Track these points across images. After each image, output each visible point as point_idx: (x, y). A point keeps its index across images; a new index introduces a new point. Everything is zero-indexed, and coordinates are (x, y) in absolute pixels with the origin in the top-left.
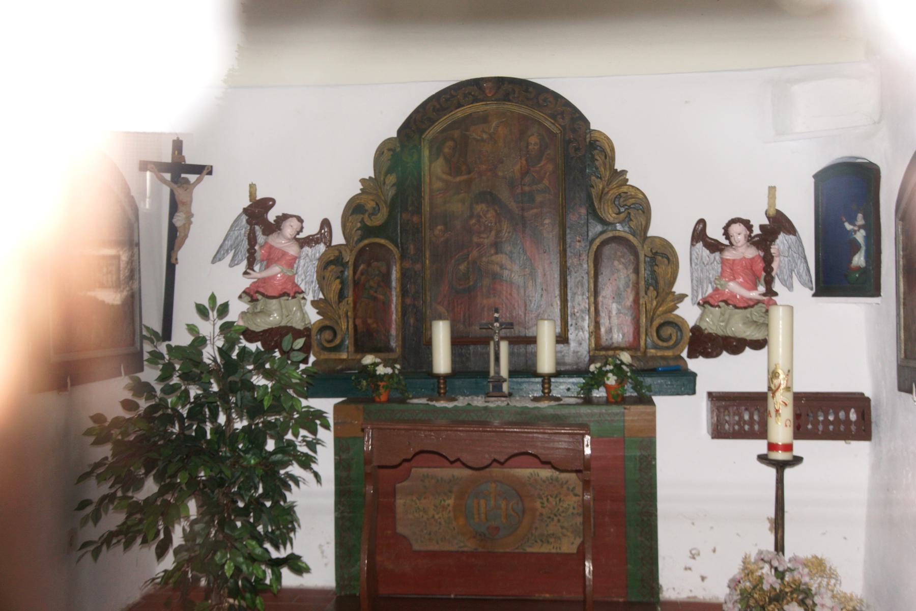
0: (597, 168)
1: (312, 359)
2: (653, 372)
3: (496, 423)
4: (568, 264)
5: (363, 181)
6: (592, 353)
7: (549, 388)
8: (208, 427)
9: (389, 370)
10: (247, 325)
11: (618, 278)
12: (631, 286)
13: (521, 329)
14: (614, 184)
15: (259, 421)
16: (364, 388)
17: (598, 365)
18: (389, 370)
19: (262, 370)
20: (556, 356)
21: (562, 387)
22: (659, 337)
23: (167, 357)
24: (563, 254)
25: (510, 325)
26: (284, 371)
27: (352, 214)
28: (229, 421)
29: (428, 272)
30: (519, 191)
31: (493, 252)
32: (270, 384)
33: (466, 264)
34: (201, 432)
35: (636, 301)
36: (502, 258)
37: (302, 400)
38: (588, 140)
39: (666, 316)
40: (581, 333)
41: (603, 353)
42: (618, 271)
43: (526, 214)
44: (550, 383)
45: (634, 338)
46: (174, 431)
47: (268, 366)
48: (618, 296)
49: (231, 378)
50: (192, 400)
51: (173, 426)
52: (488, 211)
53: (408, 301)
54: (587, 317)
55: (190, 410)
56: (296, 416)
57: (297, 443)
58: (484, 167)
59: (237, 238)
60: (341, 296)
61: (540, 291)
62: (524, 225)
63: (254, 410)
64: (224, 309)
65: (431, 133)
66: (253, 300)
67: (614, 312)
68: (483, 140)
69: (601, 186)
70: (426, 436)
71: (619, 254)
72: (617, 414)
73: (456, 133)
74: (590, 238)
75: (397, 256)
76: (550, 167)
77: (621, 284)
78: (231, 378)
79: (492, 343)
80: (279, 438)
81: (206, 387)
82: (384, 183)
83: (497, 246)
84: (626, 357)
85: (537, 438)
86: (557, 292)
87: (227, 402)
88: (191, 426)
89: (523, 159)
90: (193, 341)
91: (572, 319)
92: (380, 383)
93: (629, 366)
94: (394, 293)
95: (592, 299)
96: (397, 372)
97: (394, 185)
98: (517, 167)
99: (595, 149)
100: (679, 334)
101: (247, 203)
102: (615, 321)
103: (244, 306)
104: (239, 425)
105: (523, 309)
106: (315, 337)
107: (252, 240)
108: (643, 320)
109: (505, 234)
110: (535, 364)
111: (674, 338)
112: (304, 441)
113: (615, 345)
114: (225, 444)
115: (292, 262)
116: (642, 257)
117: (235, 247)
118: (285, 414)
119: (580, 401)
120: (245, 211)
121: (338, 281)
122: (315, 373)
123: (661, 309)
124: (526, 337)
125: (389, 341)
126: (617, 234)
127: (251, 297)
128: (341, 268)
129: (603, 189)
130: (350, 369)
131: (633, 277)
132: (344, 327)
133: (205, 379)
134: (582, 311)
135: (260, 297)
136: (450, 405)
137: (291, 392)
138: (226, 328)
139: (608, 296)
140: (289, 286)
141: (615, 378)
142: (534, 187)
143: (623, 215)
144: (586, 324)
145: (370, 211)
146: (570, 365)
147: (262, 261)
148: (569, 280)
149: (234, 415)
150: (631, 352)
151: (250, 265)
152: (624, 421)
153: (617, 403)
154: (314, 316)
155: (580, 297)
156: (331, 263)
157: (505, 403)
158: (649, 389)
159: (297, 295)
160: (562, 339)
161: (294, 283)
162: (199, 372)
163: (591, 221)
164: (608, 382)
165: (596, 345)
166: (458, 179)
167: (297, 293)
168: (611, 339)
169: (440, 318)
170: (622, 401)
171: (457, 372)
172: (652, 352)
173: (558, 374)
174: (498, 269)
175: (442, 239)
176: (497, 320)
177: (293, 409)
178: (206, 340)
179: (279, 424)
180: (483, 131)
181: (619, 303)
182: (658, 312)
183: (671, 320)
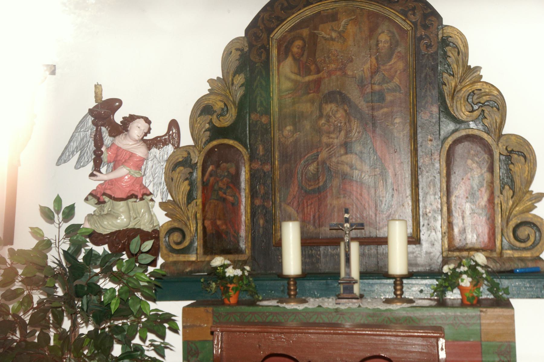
0: (449, 65)
1: (160, 261)
2: (510, 273)
3: (348, 325)
4: (420, 164)
5: (211, 81)
6: (445, 254)
7: (401, 290)
8: (52, 333)
9: (239, 272)
10: (93, 228)
11: (471, 177)
12: (485, 185)
13: (372, 229)
14: (467, 81)
15: (106, 326)
16: (213, 290)
17: (452, 266)
18: (239, 272)
19: (109, 273)
20: (408, 257)
21: (414, 289)
22: (516, 237)
23: (9, 261)
24: (415, 153)
25: (361, 226)
26: (131, 274)
27: (200, 115)
28: (75, 326)
29: (277, 173)
30: (369, 90)
31: (342, 151)
32: (117, 288)
33: (315, 164)
34: (45, 338)
35: (491, 201)
36: (352, 158)
37: (150, 303)
38: (440, 36)
39: (523, 216)
40: (434, 233)
41: (456, 254)
42: (472, 169)
43: (376, 114)
44: (402, 284)
45: (490, 238)
46: (15, 338)
47: (115, 269)
48: (472, 196)
49: (78, 282)
50: (35, 305)
51: (14, 333)
52: (337, 111)
53: (258, 202)
54: (440, 218)
55: (32, 315)
56: (144, 319)
57: (145, 348)
58: (333, 66)
59: (82, 140)
60: (190, 197)
61: (391, 191)
62: (374, 125)
63: (101, 314)
64: (70, 212)
65: (278, 33)
66: (100, 202)
67: (468, 212)
68: (332, 39)
69: (453, 84)
70: (276, 338)
71: (472, 152)
72: (473, 317)
73: (305, 32)
74: (442, 137)
75: (246, 157)
76: (401, 65)
77: (475, 183)
78: (78, 282)
79: (342, 245)
80: (126, 342)
81: (50, 291)
82: (233, 84)
83: (346, 146)
84: (481, 258)
85: (390, 340)
86: (408, 192)
87: (73, 306)
88: (33, 333)
89: (373, 58)
90: (37, 245)
91: (424, 219)
92: (229, 285)
93: (485, 267)
94: (243, 194)
95: (445, 199)
96: (246, 273)
97: (242, 85)
98: (368, 65)
99: (448, 45)
100: (537, 234)
101: (92, 104)
102: (469, 220)
103: (91, 209)
104: (85, 330)
105: (373, 209)
106: (163, 240)
107: (98, 142)
108: (499, 220)
109: (354, 134)
110: (386, 265)
111: (532, 239)
112: (151, 345)
113: (469, 246)
114: (69, 351)
115: (139, 164)
116: (496, 156)
117: (82, 149)
118: (132, 318)
119: (433, 303)
120: (91, 112)
121: (186, 183)
122: (164, 275)
123: (517, 209)
124: (376, 238)
125: (238, 242)
126: (470, 132)
127: (98, 199)
128: (189, 170)
129: (456, 86)
130: (199, 272)
131: (487, 176)
132: (193, 229)
133: (49, 284)
134: (435, 211)
135: (107, 199)
136: (301, 307)
137: (138, 295)
138: (72, 231)
139: (462, 196)
140: (137, 188)
141: (470, 279)
142: (385, 86)
143: (476, 113)
144: (438, 224)
145: (219, 112)
146: (422, 266)
147: (109, 162)
148: (420, 180)
149: (79, 320)
150: (487, 254)
151: (97, 166)
152: (480, 325)
153: (472, 306)
154: (162, 218)
155: (432, 197)
156: (180, 164)
157: (357, 305)
158: (506, 291)
159: (145, 197)
160: (414, 239)
161: (141, 185)
162: (43, 276)
163: (443, 119)
164: (463, 284)
165: (449, 246)
166: (307, 79)
167: (144, 195)
168: (465, 239)
169: (290, 218)
170: (478, 303)
171: (310, 272)
172: (508, 253)
173: (410, 275)
174: (349, 169)
175: (291, 140)
176: (347, 220)
177: (141, 312)
178: (51, 244)
179: (126, 327)
180: (333, 30)
181: (473, 203)
182: (514, 212)
183: (529, 220)
